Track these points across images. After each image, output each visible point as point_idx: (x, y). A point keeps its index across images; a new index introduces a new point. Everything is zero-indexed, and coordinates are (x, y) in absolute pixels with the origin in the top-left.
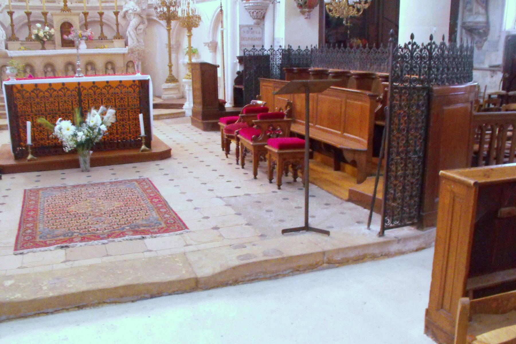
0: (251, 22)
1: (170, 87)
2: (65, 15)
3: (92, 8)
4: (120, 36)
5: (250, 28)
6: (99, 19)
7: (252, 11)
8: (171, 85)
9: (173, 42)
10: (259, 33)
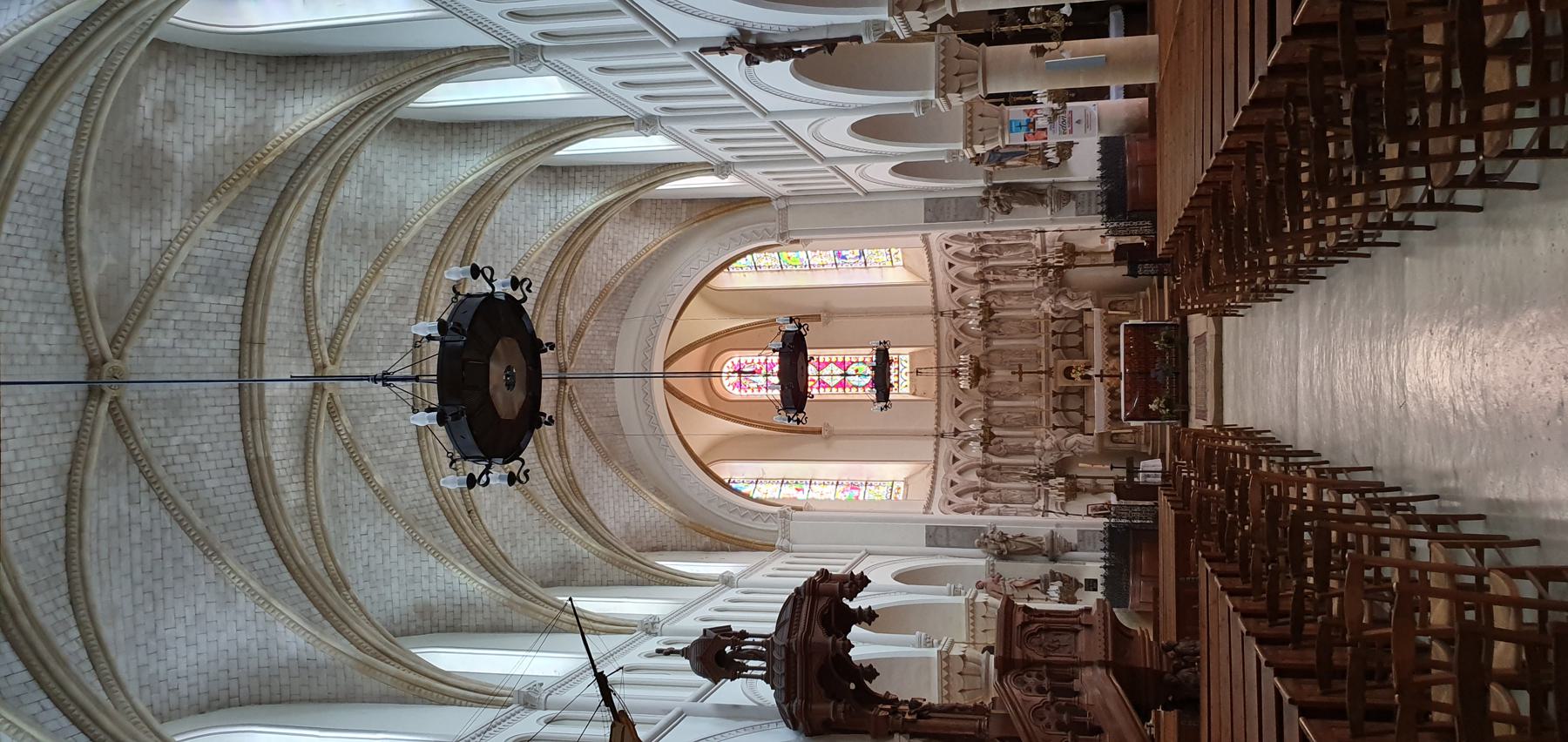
3: (1047, 341)
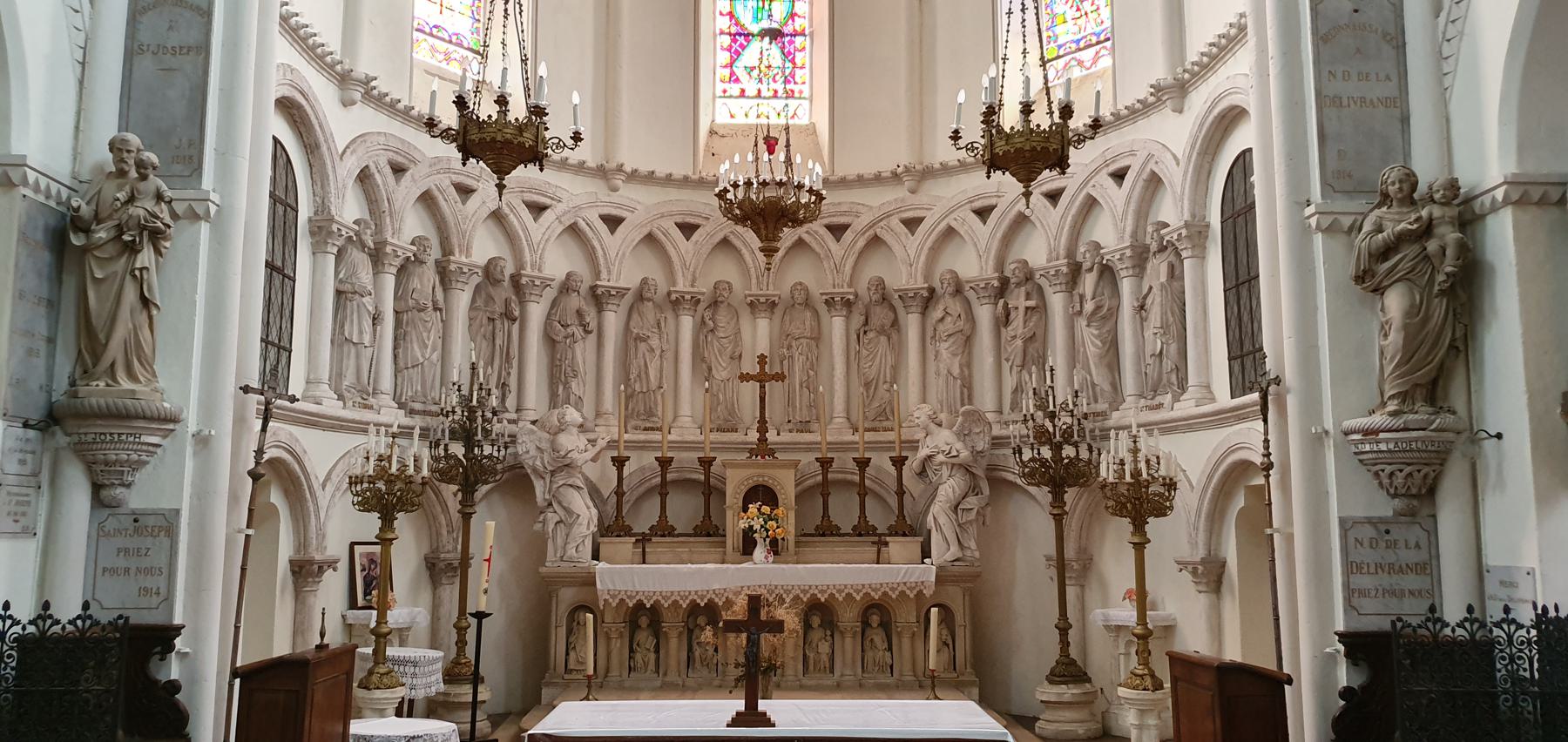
0: (1385, 507)
1: (1066, 698)
2: (759, 466)
4: (909, 527)
5: (1383, 528)
6: (857, 478)
7: (1388, 469)
8: (1068, 692)
9: (1070, 552)
10: (1418, 546)
